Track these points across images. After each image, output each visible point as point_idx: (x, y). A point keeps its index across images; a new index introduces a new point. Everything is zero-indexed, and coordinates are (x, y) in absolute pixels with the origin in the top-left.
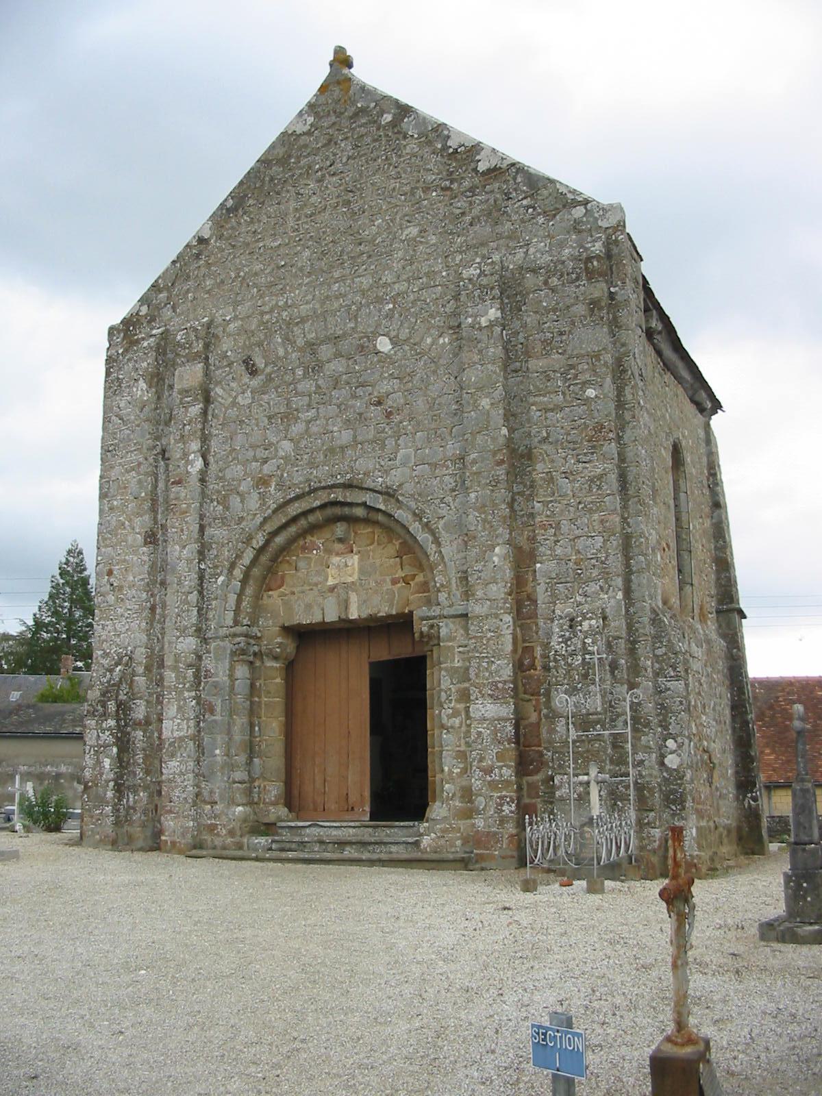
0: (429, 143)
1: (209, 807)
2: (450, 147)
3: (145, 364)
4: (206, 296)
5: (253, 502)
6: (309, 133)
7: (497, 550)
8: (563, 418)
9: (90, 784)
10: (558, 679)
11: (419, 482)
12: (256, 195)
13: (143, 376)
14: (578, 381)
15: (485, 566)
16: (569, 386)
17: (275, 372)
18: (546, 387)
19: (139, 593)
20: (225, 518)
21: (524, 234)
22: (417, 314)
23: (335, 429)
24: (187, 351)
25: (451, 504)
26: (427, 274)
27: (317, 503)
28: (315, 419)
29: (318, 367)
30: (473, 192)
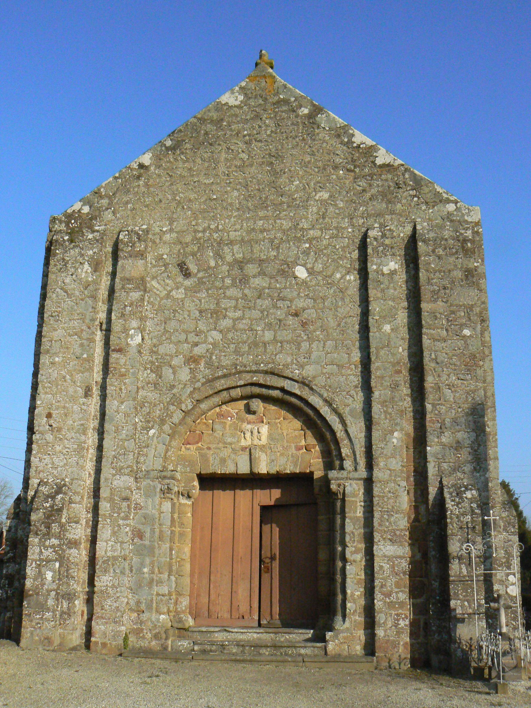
0: (338, 136)
1: (136, 614)
2: (354, 142)
3: (91, 252)
4: (144, 209)
5: (184, 375)
6: (239, 107)
7: (396, 434)
8: (446, 347)
9: (31, 592)
10: (454, 531)
11: (329, 378)
12: (192, 142)
13: (88, 261)
14: (457, 323)
15: (386, 444)
16: (451, 325)
17: (206, 277)
18: (434, 323)
19: (78, 435)
20: (158, 384)
21: (411, 215)
22: (329, 255)
23: (259, 328)
24: (130, 248)
25: (355, 397)
26: (336, 228)
27: (242, 383)
28: (241, 318)
29: (244, 280)
30: (372, 178)
